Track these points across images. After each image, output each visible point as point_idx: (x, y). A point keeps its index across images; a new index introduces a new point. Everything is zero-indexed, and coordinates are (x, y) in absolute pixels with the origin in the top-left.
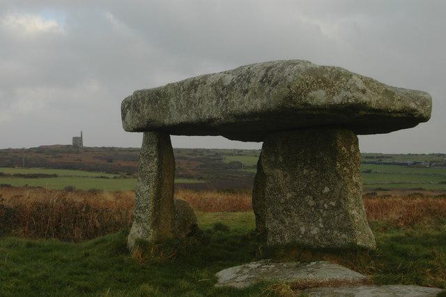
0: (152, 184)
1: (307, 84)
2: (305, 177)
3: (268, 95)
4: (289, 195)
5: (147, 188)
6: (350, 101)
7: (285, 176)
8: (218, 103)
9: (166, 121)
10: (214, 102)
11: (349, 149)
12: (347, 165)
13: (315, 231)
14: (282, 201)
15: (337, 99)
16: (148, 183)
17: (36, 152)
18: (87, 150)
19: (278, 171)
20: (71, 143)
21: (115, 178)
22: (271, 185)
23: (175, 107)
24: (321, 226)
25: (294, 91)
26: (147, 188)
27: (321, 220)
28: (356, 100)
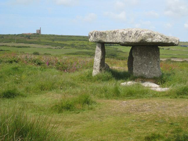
0: (100, 58)
3: (137, 39)
4: (140, 64)
8: (122, 38)
9: (105, 41)
10: (121, 38)
12: (156, 56)
13: (147, 74)
15: (154, 41)
18: (43, 36)
20: (36, 32)
21: (55, 48)
24: (148, 72)
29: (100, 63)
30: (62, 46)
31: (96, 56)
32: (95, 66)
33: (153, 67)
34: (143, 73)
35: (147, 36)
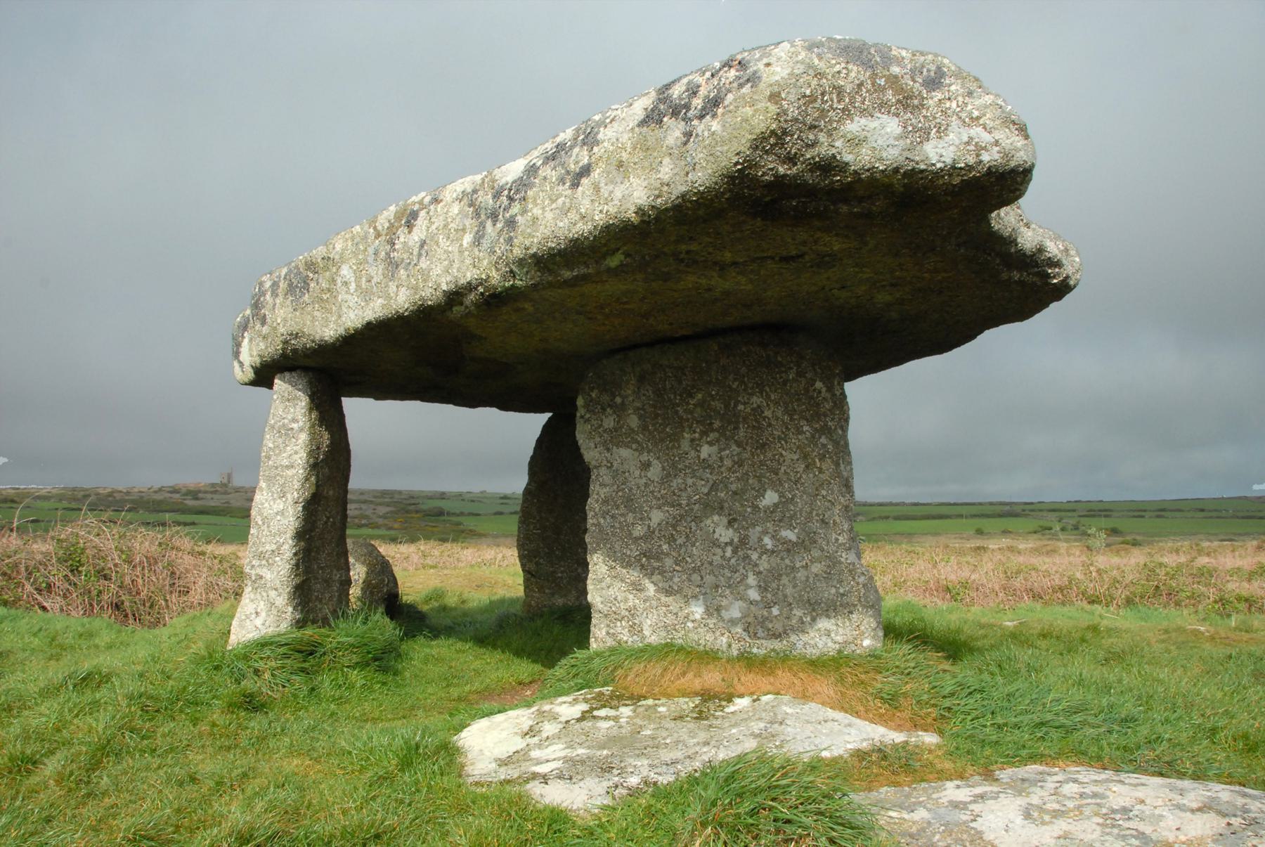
0: (293, 495)
2: (705, 464)
4: (657, 517)
5: (279, 505)
6: (986, 157)
7: (646, 466)
11: (830, 389)
14: (639, 531)
16: (283, 495)
17: (169, 492)
19: (625, 452)
22: (604, 492)
23: (353, 287)
24: (754, 594)
25: (793, 112)
26: (279, 505)
27: (752, 580)
28: (1006, 155)
31: (269, 479)
32: (261, 556)
33: (806, 543)
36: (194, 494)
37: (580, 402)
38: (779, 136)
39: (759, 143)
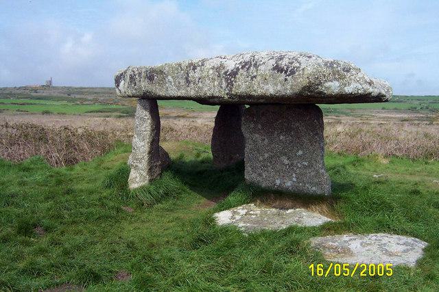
1: (325, 76)
4: (266, 155)
6: (360, 92)
9: (162, 93)
10: (216, 83)
18: (55, 88)
24: (294, 179)
26: (143, 144)
27: (294, 175)
28: (365, 91)
29: (149, 153)
30: (83, 101)
34: (278, 182)
35: (328, 71)
36: (35, 90)
37: (243, 119)
38: (309, 87)
39: (304, 88)
